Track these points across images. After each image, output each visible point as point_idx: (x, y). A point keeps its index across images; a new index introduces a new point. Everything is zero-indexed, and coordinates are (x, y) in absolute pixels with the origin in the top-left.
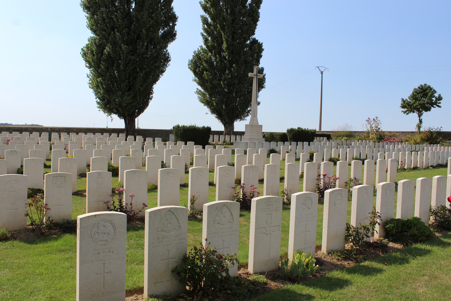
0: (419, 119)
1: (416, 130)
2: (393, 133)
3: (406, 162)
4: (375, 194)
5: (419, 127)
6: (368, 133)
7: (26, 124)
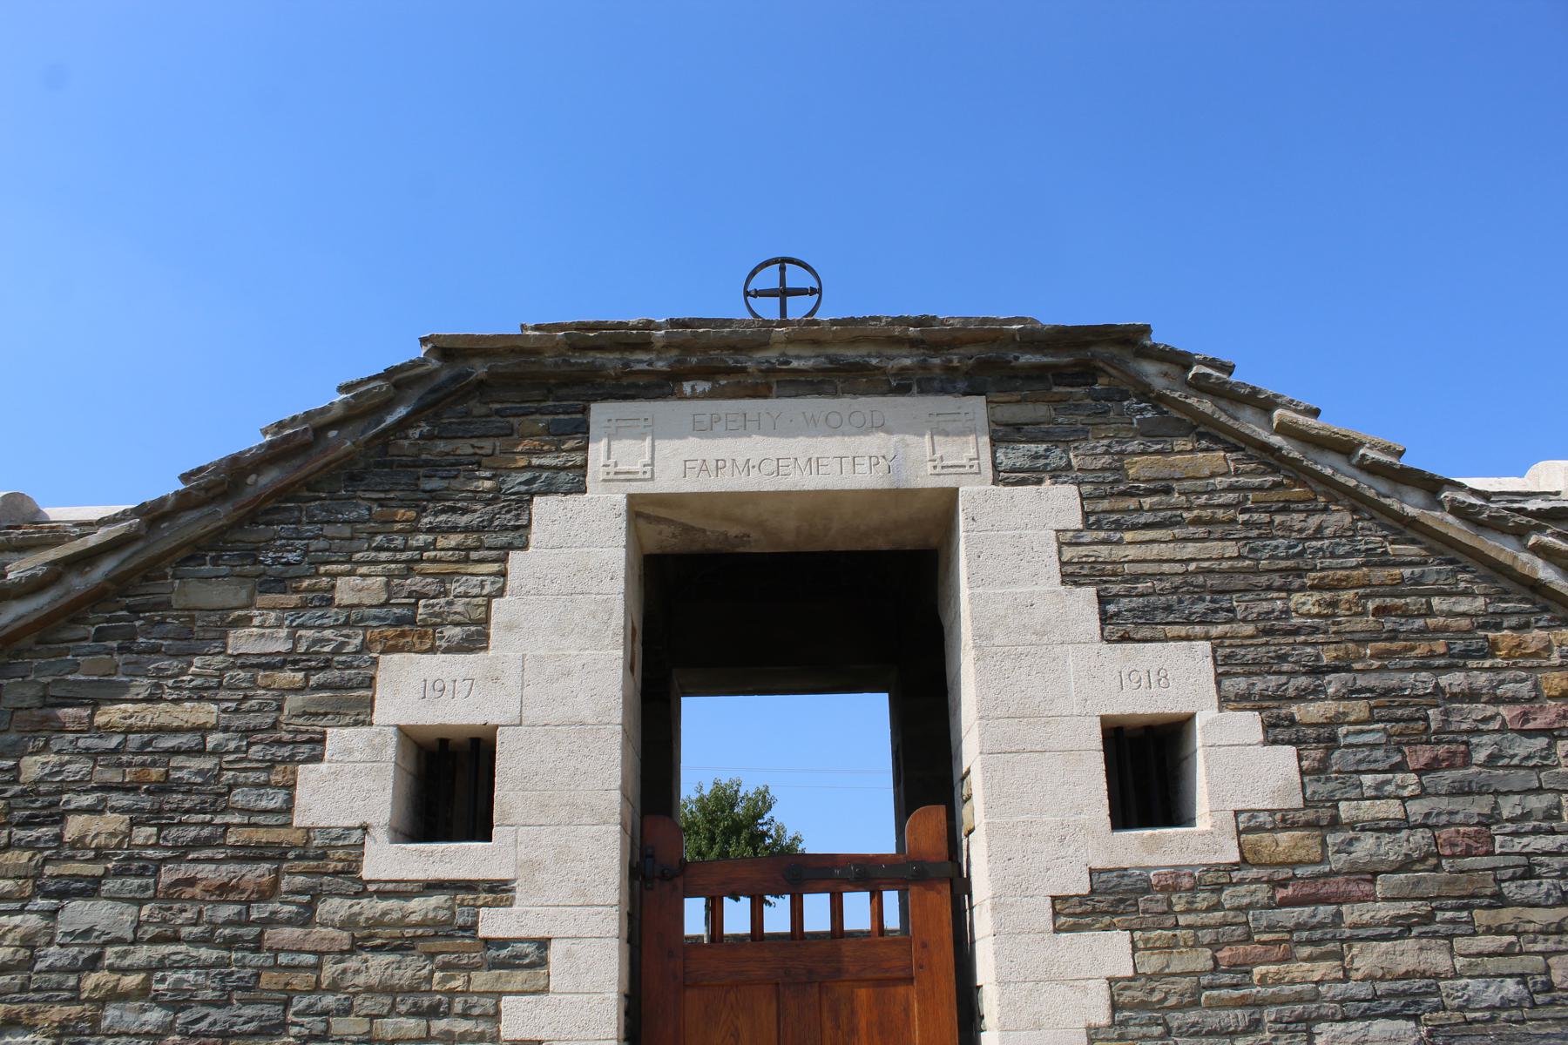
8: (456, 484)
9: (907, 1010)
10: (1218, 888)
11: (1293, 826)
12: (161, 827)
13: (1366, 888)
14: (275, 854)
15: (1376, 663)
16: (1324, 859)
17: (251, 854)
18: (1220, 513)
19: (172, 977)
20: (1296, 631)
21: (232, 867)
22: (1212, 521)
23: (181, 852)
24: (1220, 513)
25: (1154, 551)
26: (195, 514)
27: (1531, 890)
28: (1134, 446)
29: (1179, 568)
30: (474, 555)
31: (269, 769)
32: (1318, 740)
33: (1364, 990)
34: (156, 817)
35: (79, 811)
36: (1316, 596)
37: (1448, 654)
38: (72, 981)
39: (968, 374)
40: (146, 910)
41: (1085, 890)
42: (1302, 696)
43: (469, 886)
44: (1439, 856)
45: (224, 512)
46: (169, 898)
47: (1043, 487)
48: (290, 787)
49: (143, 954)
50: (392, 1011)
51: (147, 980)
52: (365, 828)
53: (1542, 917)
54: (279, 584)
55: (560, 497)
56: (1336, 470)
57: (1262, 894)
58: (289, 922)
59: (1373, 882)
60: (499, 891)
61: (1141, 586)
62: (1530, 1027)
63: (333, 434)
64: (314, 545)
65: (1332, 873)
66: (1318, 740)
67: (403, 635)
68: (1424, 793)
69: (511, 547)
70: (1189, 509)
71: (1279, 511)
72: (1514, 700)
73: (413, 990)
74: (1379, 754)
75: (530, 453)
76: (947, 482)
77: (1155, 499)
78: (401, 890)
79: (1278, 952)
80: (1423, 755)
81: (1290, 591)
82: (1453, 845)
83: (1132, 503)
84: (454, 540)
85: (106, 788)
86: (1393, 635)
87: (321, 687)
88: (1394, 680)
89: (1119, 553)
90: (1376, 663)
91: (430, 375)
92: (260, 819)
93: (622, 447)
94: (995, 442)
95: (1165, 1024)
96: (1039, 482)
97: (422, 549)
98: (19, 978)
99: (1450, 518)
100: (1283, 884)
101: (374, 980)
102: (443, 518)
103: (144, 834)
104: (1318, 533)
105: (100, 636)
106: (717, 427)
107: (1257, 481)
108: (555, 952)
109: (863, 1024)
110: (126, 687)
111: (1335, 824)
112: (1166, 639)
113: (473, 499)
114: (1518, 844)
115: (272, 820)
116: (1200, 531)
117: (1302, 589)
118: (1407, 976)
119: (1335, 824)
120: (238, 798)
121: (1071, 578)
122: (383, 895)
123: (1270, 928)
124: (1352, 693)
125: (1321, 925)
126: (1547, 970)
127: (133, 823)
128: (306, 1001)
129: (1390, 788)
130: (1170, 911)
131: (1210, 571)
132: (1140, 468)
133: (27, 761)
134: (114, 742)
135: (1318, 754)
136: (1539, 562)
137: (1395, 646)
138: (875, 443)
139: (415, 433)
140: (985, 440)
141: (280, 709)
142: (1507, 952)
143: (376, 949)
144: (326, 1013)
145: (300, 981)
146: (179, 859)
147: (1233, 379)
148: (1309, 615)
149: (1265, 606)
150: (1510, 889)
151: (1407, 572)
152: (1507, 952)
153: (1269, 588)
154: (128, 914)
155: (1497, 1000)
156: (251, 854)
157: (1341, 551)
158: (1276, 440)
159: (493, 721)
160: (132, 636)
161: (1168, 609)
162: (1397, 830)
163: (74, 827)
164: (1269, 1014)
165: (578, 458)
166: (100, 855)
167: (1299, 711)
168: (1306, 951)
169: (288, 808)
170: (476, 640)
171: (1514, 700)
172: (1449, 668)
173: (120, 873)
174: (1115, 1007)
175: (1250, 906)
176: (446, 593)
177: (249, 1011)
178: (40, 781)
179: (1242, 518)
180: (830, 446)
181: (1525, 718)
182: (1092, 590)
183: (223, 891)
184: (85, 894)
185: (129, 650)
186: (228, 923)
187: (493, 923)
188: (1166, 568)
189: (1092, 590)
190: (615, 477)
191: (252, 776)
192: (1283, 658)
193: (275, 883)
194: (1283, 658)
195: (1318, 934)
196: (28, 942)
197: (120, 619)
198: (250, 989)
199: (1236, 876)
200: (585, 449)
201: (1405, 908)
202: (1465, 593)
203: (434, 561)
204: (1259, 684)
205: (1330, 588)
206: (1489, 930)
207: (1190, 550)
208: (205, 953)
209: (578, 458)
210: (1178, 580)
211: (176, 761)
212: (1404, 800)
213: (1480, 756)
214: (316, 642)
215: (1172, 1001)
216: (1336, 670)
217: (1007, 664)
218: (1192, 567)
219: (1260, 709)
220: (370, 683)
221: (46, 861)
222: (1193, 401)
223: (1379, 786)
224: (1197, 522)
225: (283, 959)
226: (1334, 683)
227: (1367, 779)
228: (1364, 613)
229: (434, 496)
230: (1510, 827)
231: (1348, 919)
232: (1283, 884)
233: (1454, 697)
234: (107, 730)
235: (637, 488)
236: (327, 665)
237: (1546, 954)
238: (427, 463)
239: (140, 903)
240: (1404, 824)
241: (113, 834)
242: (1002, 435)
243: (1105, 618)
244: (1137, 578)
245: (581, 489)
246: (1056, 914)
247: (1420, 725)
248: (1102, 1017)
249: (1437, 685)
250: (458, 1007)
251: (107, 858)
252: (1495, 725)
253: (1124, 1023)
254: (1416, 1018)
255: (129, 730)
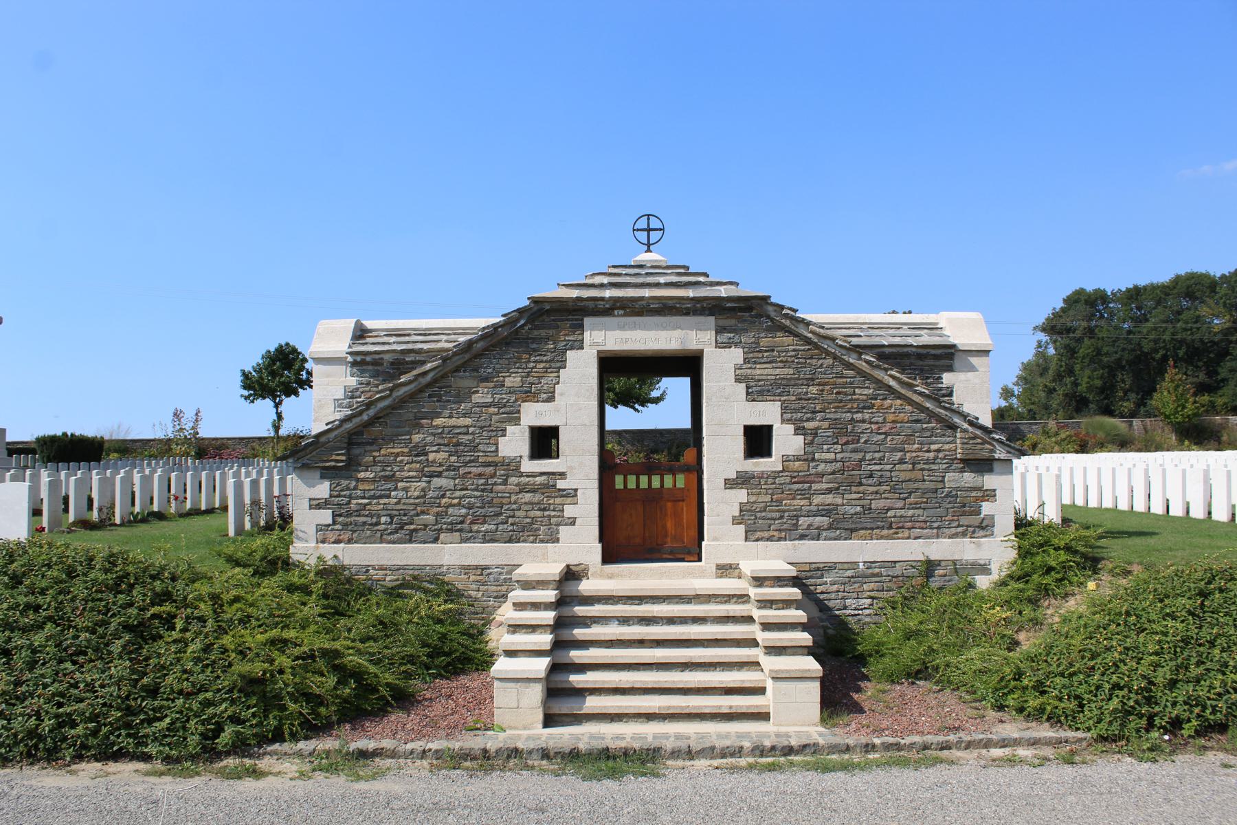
0: (277, 413)
1: (272, 434)
2: (219, 441)
3: (189, 495)
4: (542, 606)
5: (277, 427)
6: (168, 442)
7: (734, 518)
8: (541, 346)
9: (682, 509)
10: (775, 478)
11: (800, 460)
12: (458, 457)
13: (820, 479)
14: (494, 464)
15: (834, 410)
16: (808, 470)
17: (488, 464)
18: (789, 359)
19: (467, 500)
20: (809, 399)
21: (481, 468)
22: (787, 361)
23: (466, 464)
24: (789, 359)
25: (766, 372)
26: (458, 357)
27: (870, 481)
28: (763, 335)
29: (773, 377)
30: (549, 370)
31: (489, 439)
32: (811, 434)
33: (815, 509)
34: (456, 453)
35: (432, 452)
36: (817, 388)
37: (858, 408)
38: (438, 501)
39: (710, 309)
40: (457, 481)
41: (735, 477)
42: (808, 420)
43: (553, 474)
44: (844, 471)
45: (467, 356)
46: (463, 477)
47: (731, 349)
48: (497, 444)
49: (458, 493)
50: (533, 509)
51: (460, 501)
52: (521, 457)
53: (871, 489)
54: (486, 380)
55: (575, 351)
56: (828, 346)
57: (788, 480)
58: (500, 484)
59: (822, 477)
60: (562, 475)
61: (760, 383)
62: (862, 520)
63: (500, 329)
64: (497, 366)
65: (810, 475)
66: (811, 434)
67: (528, 396)
68: (842, 451)
69: (560, 368)
70: (779, 357)
71: (809, 358)
72: (877, 423)
73: (538, 503)
74: (830, 439)
75: (565, 335)
76: (700, 347)
77: (768, 354)
78: (533, 475)
79: (790, 497)
80: (844, 439)
81: (809, 386)
82: (848, 467)
83: (760, 355)
84: (542, 365)
85: (439, 445)
86: (841, 401)
87: (503, 413)
88: (838, 416)
89: (754, 372)
90: (834, 410)
91: (531, 309)
92: (488, 454)
93: (595, 333)
94: (717, 333)
95: (755, 516)
96: (730, 347)
97: (532, 368)
98: (422, 500)
99: (864, 364)
100: (795, 477)
101: (527, 501)
102: (538, 358)
103: (453, 459)
104: (821, 366)
105: (430, 396)
106: (626, 327)
107: (803, 348)
108: (579, 493)
109: (669, 513)
110: (441, 413)
111: (813, 460)
112: (767, 401)
113: (547, 351)
114: (869, 468)
115: (492, 454)
116: (782, 365)
117: (813, 385)
118: (828, 505)
119: (813, 460)
120: (481, 447)
121: (738, 380)
122: (528, 476)
123: (789, 490)
124: (824, 420)
125: (805, 490)
126: (871, 504)
127: (450, 456)
128: (507, 507)
129: (832, 450)
130: (760, 484)
131: (784, 378)
132: (765, 342)
133: (413, 437)
134: (440, 431)
135: (811, 438)
136: (891, 379)
137: (841, 404)
138: (677, 333)
139: (526, 328)
140: (714, 332)
141: (491, 420)
142: (860, 499)
143: (526, 492)
144: (513, 510)
145: (505, 501)
146: (465, 466)
147: (797, 315)
148: (814, 394)
149: (800, 390)
150: (864, 481)
151: (848, 380)
152: (860, 499)
153: (802, 385)
154: (452, 482)
155: (853, 512)
156: (488, 464)
157: (828, 372)
158: (810, 335)
159: (558, 424)
160: (440, 396)
161: (769, 391)
162: (832, 462)
163: (431, 457)
164: (786, 514)
165: (580, 337)
166: (441, 465)
167: (806, 425)
168: (799, 497)
169: (497, 451)
170: (551, 399)
171: (877, 423)
172: (857, 412)
173: (447, 470)
174: (741, 511)
175: (784, 483)
176: (541, 383)
177: (491, 510)
178: (419, 442)
179: (796, 360)
180: (663, 334)
181: (879, 428)
182: (744, 384)
183: (480, 475)
184: (437, 476)
185: (440, 401)
186: (481, 485)
187: (561, 484)
188: (769, 377)
189: (744, 384)
190: (593, 344)
191: (485, 441)
192: (804, 408)
193: (495, 473)
194: (804, 408)
195: (803, 492)
196: (423, 490)
197: (436, 391)
198: (490, 503)
199: (781, 474)
200: (583, 334)
201: (831, 485)
202: (867, 388)
203: (536, 372)
204: (795, 416)
205: (822, 385)
206: (855, 493)
207: (778, 371)
208: (476, 493)
209: (580, 337)
210: (773, 382)
211: (460, 437)
212: (836, 453)
213: (862, 441)
214: (500, 399)
215: (758, 510)
216: (821, 412)
217: (716, 408)
218: (778, 377)
219: (794, 424)
220: (519, 412)
221: (425, 466)
222: (783, 321)
223: (828, 449)
224: (781, 361)
225: (499, 495)
226: (819, 416)
227: (825, 447)
228: (832, 394)
229: (534, 350)
230: (868, 462)
231: (813, 488)
232: (795, 477)
233: (857, 422)
234: (437, 427)
235: (600, 348)
236: (505, 406)
237: (871, 500)
238: (531, 338)
239: (455, 479)
240: (835, 460)
241: (444, 459)
242: (719, 330)
243: (748, 393)
244: (759, 380)
245: (582, 348)
246: (726, 484)
247: (845, 430)
248: (737, 514)
249: (852, 418)
250: (552, 508)
251: (443, 466)
252: (869, 431)
253: (743, 515)
254: (829, 517)
255: (444, 427)
